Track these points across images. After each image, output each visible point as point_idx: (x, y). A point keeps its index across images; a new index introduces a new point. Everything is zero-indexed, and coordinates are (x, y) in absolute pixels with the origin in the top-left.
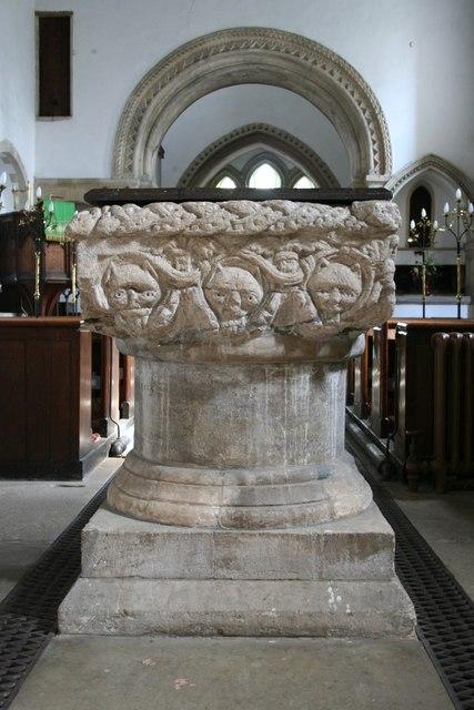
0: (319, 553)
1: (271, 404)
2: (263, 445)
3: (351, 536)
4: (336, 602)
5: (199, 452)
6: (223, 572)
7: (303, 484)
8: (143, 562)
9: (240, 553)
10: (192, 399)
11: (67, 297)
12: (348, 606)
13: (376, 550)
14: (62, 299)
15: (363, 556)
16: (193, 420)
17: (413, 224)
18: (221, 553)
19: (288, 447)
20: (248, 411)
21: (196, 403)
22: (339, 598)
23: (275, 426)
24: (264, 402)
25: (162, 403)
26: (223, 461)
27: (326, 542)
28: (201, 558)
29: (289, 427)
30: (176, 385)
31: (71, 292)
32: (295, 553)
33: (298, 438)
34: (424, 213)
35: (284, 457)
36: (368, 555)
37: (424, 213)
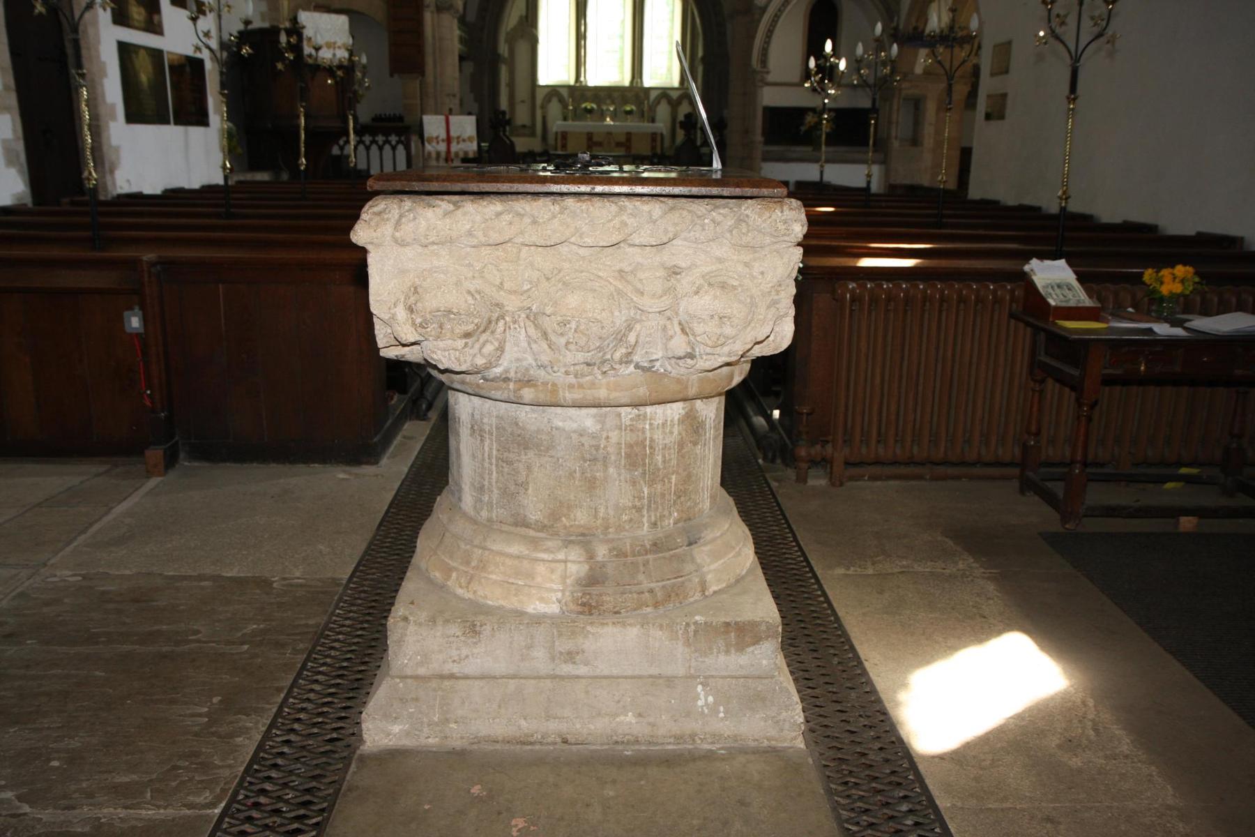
0: (687, 643)
1: (628, 456)
2: (617, 507)
3: (727, 624)
4: (707, 704)
5: (535, 513)
6: (567, 669)
7: (667, 554)
8: (467, 656)
9: (589, 645)
10: (526, 448)
11: (342, 148)
12: (722, 709)
13: (757, 640)
14: (336, 151)
15: (741, 647)
16: (527, 476)
17: (812, 63)
18: (563, 645)
19: (649, 507)
20: (599, 465)
21: (531, 454)
22: (711, 699)
23: (634, 483)
24: (619, 453)
25: (486, 449)
26: (565, 527)
27: (696, 632)
28: (540, 654)
29: (651, 483)
30: (504, 429)
31: (347, 142)
32: (657, 645)
33: (663, 495)
34: (828, 46)
35: (645, 520)
36: (748, 646)
37: (828, 46)
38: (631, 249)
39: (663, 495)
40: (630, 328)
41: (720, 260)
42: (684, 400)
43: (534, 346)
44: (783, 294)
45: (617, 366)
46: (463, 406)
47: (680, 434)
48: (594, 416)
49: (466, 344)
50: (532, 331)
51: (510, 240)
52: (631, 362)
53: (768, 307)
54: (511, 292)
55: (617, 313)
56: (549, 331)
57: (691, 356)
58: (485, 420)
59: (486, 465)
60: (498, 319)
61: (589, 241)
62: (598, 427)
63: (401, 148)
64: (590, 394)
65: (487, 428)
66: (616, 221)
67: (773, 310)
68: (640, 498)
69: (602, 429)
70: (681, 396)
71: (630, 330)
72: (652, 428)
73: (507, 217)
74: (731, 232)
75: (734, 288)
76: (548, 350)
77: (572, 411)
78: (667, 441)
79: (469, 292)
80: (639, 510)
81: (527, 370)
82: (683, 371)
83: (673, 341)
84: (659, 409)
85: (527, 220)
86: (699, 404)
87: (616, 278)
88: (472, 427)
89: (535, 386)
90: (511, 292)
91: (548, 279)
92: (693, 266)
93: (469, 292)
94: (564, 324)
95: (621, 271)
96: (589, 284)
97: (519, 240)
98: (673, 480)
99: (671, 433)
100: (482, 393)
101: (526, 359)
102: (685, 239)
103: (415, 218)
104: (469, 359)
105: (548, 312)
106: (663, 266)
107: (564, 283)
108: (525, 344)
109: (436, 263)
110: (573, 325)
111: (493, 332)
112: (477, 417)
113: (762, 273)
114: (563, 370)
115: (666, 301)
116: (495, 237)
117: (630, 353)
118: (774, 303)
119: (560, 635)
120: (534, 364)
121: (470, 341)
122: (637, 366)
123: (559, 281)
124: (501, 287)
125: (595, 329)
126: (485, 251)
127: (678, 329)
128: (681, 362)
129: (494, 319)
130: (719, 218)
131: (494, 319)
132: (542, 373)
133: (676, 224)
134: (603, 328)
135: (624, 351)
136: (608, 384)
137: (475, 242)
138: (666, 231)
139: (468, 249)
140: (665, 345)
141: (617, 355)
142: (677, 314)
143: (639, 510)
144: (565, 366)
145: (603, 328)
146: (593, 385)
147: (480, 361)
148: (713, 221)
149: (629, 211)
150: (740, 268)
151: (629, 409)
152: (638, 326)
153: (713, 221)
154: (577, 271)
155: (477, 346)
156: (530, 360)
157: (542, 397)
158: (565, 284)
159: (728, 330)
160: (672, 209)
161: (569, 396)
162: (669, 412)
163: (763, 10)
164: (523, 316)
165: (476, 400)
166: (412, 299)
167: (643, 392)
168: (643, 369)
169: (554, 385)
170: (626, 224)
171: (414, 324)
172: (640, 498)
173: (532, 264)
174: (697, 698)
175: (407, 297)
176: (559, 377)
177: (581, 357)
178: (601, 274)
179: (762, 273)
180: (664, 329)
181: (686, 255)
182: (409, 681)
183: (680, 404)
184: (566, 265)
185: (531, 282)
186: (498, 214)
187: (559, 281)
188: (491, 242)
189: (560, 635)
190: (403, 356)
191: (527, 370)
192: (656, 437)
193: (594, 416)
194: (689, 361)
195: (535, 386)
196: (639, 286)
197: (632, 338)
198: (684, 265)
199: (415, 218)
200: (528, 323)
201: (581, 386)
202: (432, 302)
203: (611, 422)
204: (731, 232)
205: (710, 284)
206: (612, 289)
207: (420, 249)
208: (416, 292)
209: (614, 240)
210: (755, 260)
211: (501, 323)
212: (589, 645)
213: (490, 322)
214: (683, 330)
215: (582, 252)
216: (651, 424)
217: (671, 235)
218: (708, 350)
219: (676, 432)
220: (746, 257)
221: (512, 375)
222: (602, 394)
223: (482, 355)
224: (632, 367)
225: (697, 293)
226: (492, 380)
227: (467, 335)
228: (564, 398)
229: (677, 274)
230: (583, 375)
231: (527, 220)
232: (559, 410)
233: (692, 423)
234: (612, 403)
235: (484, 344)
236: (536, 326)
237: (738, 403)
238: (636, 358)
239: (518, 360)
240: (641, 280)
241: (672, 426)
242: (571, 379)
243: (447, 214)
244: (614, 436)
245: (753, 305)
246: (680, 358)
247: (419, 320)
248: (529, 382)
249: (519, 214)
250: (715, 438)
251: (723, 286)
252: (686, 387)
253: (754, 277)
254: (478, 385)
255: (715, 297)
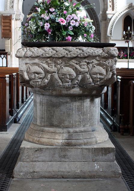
1: (78, 108)
2: (75, 121)
5: (55, 123)
6: (63, 159)
9: (69, 154)
13: (109, 152)
15: (106, 154)
16: (54, 113)
18: (62, 154)
23: (79, 115)
28: (57, 155)
29: (83, 116)
32: (85, 153)
34: (129, 28)
36: (107, 154)
37: (129, 28)
39: (86, 119)
59: (44, 112)
63: (4, 58)
68: (81, 119)
80: (80, 122)
98: (88, 115)
119: (62, 151)
143: (80, 122)
163: (110, 19)
172: (81, 119)
174: (95, 166)
182: (25, 162)
189: (62, 151)
195: (56, 91)
212: (69, 154)
250: (99, 107)
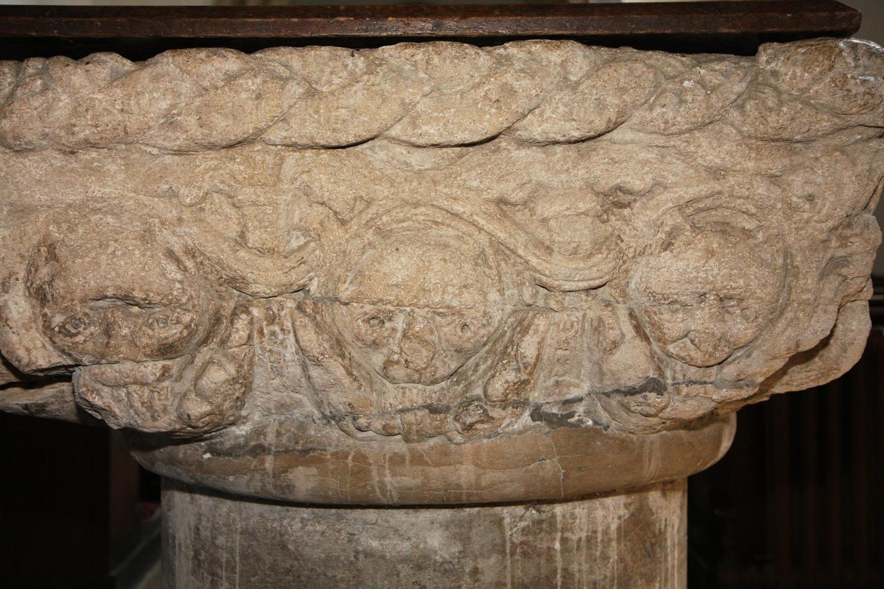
30: (258, 559)
38: (522, 154)
40: (523, 327)
41: (717, 173)
42: (629, 490)
43: (314, 372)
44: (856, 245)
45: (496, 413)
46: (183, 512)
47: (621, 560)
48: (446, 526)
49: (166, 370)
50: (309, 337)
51: (260, 132)
52: (525, 403)
53: (823, 276)
54: (264, 252)
55: (494, 296)
56: (348, 337)
57: (656, 386)
58: (221, 540)
60: (234, 314)
61: (432, 132)
62: (456, 548)
64: (437, 477)
65: (224, 556)
66: (492, 87)
67: (833, 282)
69: (463, 554)
70: (627, 478)
71: (525, 331)
72: (565, 550)
73: (252, 84)
74: (741, 108)
75: (747, 234)
76: (346, 381)
77: (399, 517)
78: (597, 576)
79: (170, 254)
81: (302, 427)
82: (635, 421)
83: (618, 356)
84: (580, 509)
85: (295, 89)
86: (654, 498)
87: (490, 216)
88: (196, 556)
89: (318, 461)
90: (264, 252)
91: (343, 223)
92: (659, 185)
93: (170, 254)
94: (378, 319)
95: (501, 201)
96: (434, 232)
97: (277, 134)
99: (605, 558)
100: (211, 481)
101: (300, 404)
102: (642, 127)
103: (45, 89)
104: (172, 404)
105: (344, 296)
106: (591, 187)
107: (379, 231)
108: (297, 370)
109: (96, 190)
110: (400, 323)
111: (223, 342)
112: (205, 533)
113: (810, 198)
114: (378, 424)
115: (600, 267)
116: (223, 127)
117: (525, 382)
118: (835, 265)
120: (317, 414)
121: (174, 365)
122: (537, 414)
123: (367, 225)
124: (242, 239)
125: (448, 330)
126: (206, 161)
127: (627, 328)
128: (631, 401)
129: (227, 312)
130: (714, 79)
131: (227, 312)
132: (334, 433)
133: (623, 90)
134: (464, 326)
135: (511, 376)
136: (477, 452)
137: (180, 140)
138: (600, 105)
139: (168, 159)
140: (599, 364)
141: (498, 387)
142: (624, 294)
144: (383, 413)
145: (464, 326)
146: (444, 456)
147: (197, 408)
148: (701, 83)
149: (518, 66)
150: (761, 189)
151: (520, 510)
152: (541, 323)
153: (701, 83)
154: (406, 203)
155: (190, 375)
156: (310, 407)
157: (335, 486)
158: (383, 233)
159: (739, 328)
160: (607, 63)
161: (392, 482)
162: (599, 513)
164: (291, 304)
165: (205, 501)
166: (44, 272)
167: (551, 468)
168: (550, 419)
169: (360, 458)
170: (512, 92)
171: (47, 328)
173: (307, 191)
175: (32, 268)
176: (374, 445)
177: (416, 394)
178: (458, 208)
179: (810, 198)
180: (598, 327)
181: (646, 162)
183: (621, 499)
184: (383, 190)
185: (306, 232)
186: (231, 79)
187: (367, 225)
188: (215, 138)
190: (42, 407)
191: (302, 427)
192: (575, 567)
193: (446, 526)
194: (652, 397)
195: (318, 461)
196: (542, 234)
197: (529, 347)
198: (637, 185)
199: (45, 89)
200: (301, 320)
201: (418, 459)
202: (89, 274)
203: (480, 537)
204: (741, 108)
205: (694, 227)
206: (483, 239)
207: (58, 160)
208: (52, 257)
209: (486, 128)
210: (793, 169)
211: (242, 322)
213: (217, 319)
214: (638, 329)
215: (417, 158)
216: (564, 541)
217: (611, 114)
218: (693, 373)
219: (614, 556)
220: (776, 163)
221: (270, 438)
222: (464, 474)
223: (200, 394)
224: (526, 418)
225: (667, 246)
226: (229, 453)
227: (166, 350)
228: (382, 484)
229: (622, 206)
230: (423, 436)
231: (295, 89)
232: (371, 515)
233: (640, 531)
234: (488, 498)
235: (204, 369)
236: (319, 327)
237: (708, 496)
238: (535, 396)
239: (282, 407)
240: (544, 221)
241: (607, 543)
242: (397, 445)
243: (116, 78)
244: (489, 566)
245: (789, 271)
246: (632, 392)
247: (58, 319)
248: (305, 453)
249: (276, 77)
251: (724, 229)
252: (639, 459)
253: (793, 208)
254: (200, 464)
255: (710, 253)
